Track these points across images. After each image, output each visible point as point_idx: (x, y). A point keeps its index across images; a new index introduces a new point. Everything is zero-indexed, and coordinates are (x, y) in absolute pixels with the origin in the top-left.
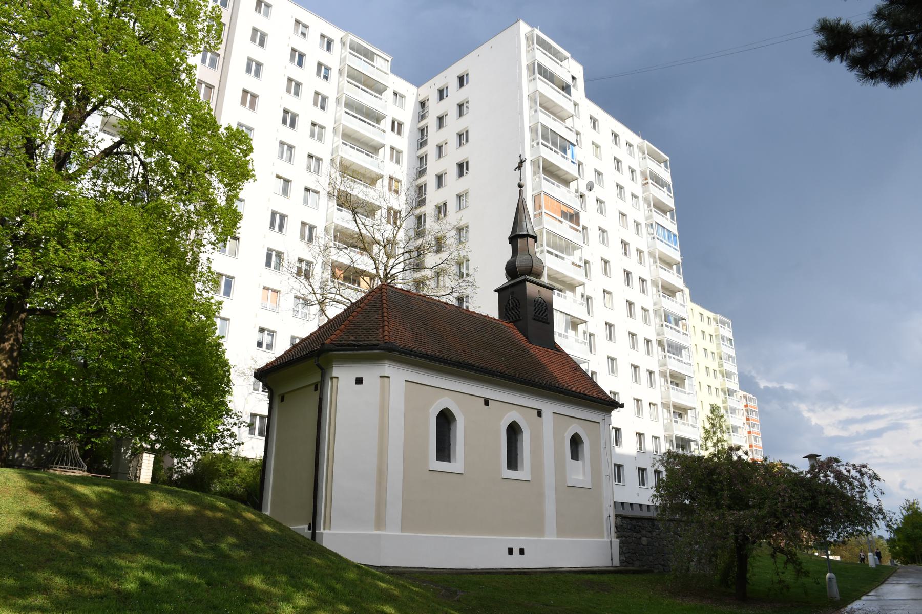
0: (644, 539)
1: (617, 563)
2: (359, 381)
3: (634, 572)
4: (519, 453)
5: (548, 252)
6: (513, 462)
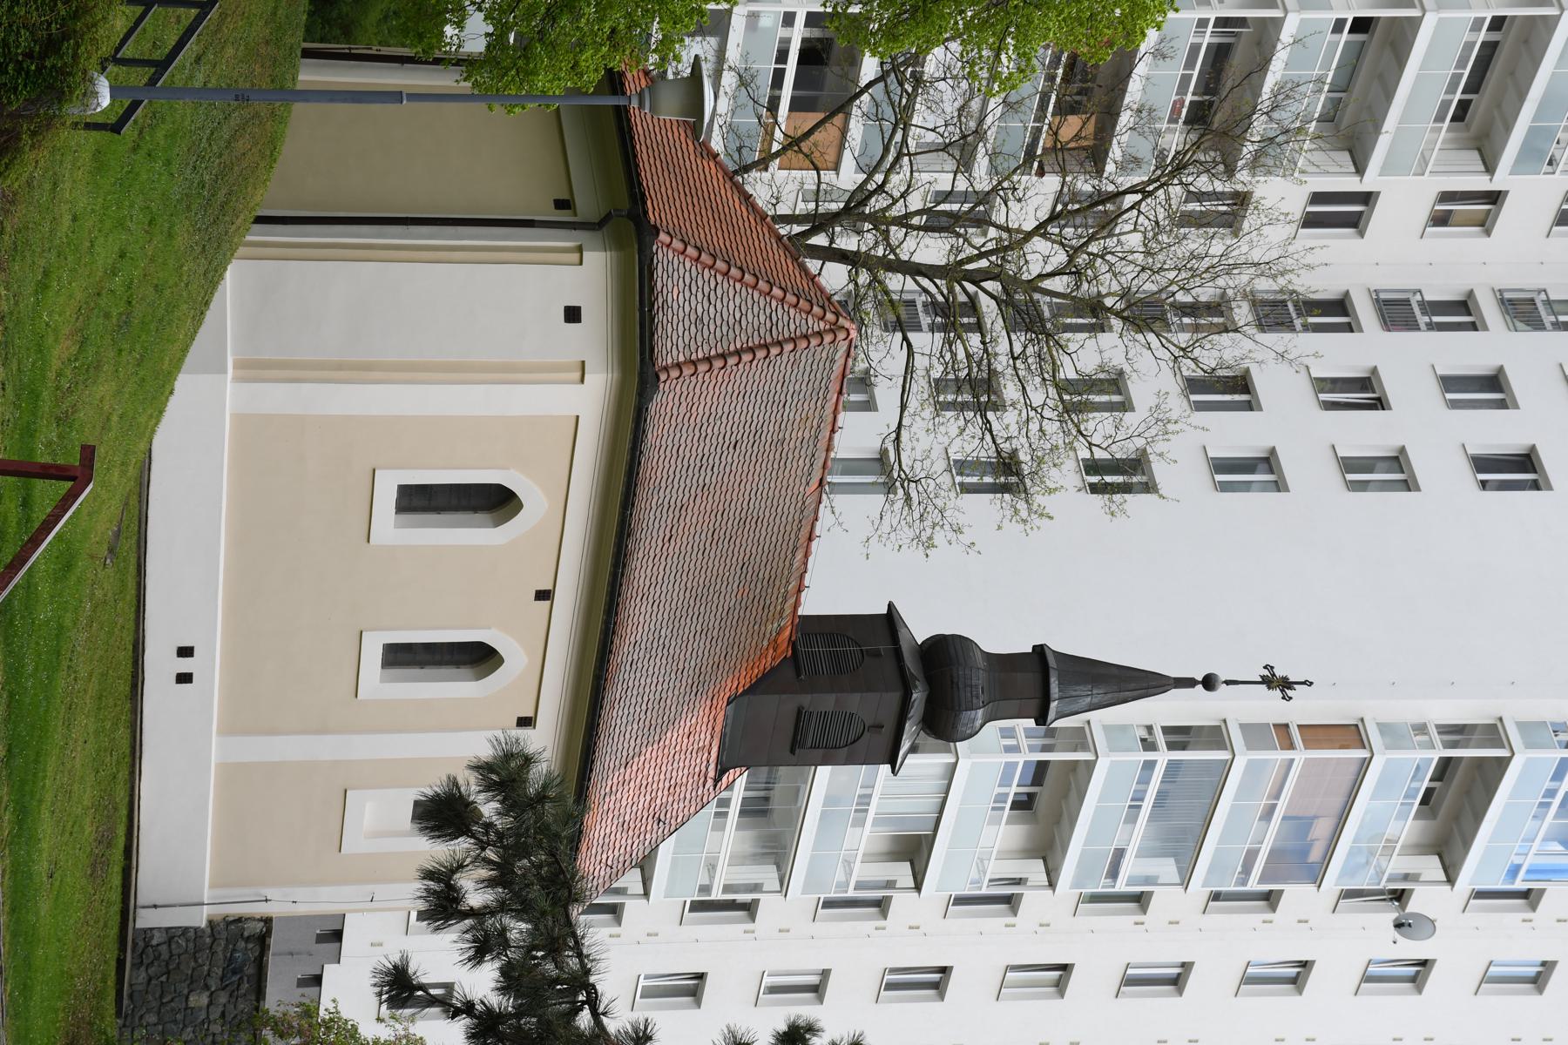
0: (204, 1000)
1: (146, 919)
2: (573, 315)
3: (121, 964)
4: (427, 671)
5: (1149, 766)
6: (400, 656)
